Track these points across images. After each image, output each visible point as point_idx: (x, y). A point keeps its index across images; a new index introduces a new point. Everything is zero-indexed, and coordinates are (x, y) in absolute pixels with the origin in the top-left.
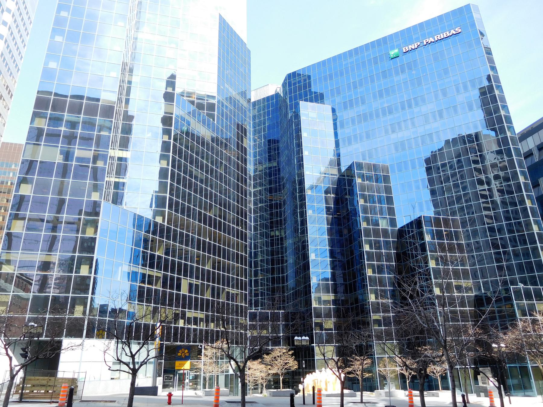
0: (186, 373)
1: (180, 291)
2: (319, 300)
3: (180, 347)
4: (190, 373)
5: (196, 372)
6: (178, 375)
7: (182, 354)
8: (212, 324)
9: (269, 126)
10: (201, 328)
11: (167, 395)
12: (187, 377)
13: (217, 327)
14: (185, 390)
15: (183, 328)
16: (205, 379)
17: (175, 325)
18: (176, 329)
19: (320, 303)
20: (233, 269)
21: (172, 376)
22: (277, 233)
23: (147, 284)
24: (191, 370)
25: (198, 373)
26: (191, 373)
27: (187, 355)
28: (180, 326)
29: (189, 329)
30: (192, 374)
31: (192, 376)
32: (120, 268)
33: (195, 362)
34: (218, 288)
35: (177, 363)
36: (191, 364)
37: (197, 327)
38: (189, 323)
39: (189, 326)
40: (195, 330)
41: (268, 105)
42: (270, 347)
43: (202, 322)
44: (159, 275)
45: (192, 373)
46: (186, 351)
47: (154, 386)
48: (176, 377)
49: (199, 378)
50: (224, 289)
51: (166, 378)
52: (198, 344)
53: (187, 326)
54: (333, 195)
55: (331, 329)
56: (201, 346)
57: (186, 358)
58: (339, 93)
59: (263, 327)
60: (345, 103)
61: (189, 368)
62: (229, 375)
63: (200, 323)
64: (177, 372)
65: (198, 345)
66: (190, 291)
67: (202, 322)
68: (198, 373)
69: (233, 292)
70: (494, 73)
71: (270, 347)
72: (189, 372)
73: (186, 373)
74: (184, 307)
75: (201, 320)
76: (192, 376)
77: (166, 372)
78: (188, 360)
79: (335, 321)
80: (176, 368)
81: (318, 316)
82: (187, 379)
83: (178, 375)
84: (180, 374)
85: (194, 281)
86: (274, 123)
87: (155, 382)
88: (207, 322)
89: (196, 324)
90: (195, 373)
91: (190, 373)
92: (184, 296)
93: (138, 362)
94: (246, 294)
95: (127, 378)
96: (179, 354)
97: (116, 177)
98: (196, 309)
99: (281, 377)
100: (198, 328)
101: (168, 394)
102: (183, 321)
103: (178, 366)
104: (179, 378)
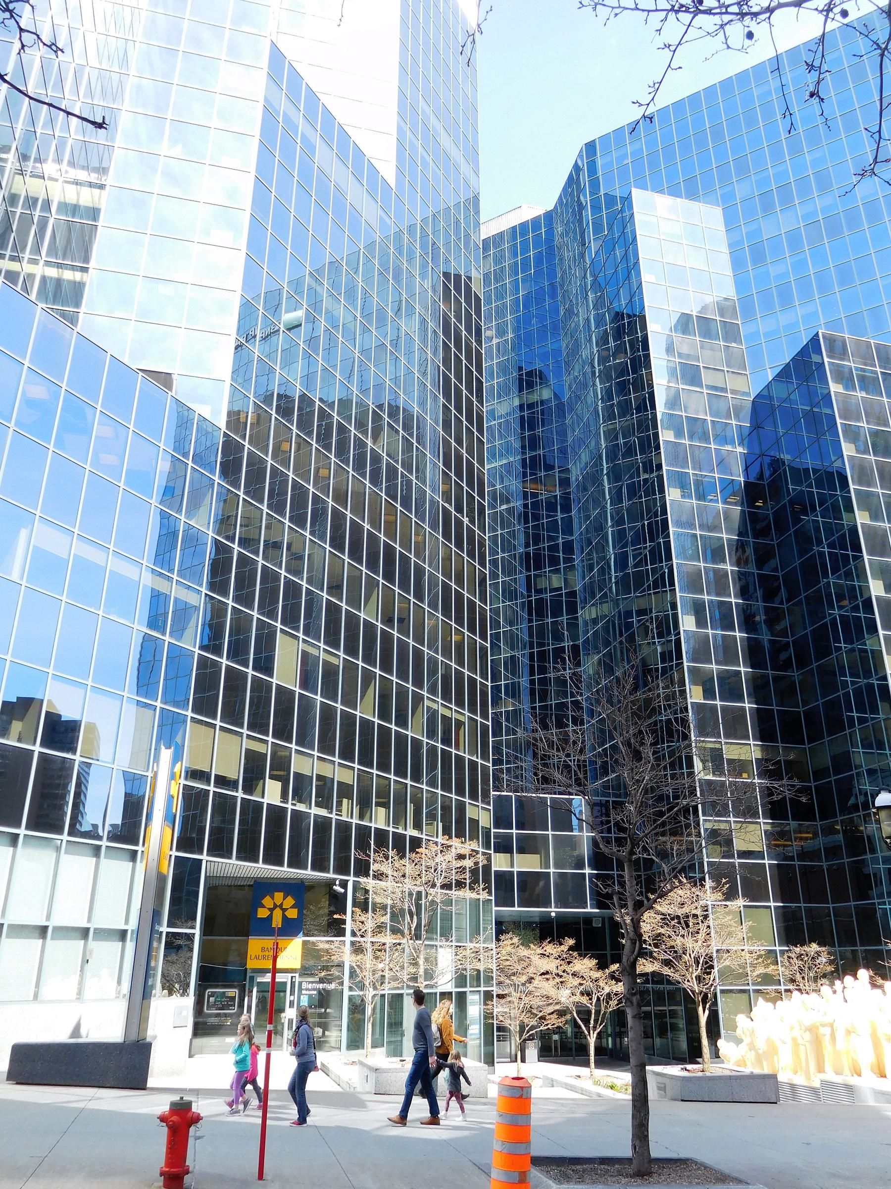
0: (285, 984)
1: (269, 671)
2: (715, 759)
3: (264, 887)
4: (300, 984)
5: (322, 981)
6: (255, 990)
7: (271, 910)
8: (382, 811)
9: (527, 298)
10: (344, 818)
11: (163, 1119)
12: (289, 998)
13: (396, 822)
14: (280, 1046)
15: (276, 814)
16: (357, 1008)
17: (251, 794)
18: (252, 810)
19: (718, 768)
20: (433, 672)
21: (233, 992)
22: (557, 581)
23: (138, 623)
24: (305, 971)
25: (332, 986)
26: (304, 986)
27: (293, 914)
28: (266, 801)
29: (298, 816)
30: (310, 988)
31: (310, 996)
32: (24, 534)
33: (321, 941)
34: (402, 693)
35: (256, 945)
36: (309, 951)
37: (331, 813)
38: (300, 795)
39: (301, 807)
40: (323, 825)
41: (525, 244)
42: (553, 909)
43: (345, 801)
44: (192, 599)
45: (310, 986)
46: (290, 901)
47: (133, 1037)
48: (250, 997)
49: (332, 1004)
50: (418, 699)
51: (212, 999)
52: (331, 875)
53: (293, 804)
54: (740, 450)
55: (760, 855)
56: (344, 884)
57: (290, 928)
58: (743, 170)
59: (527, 846)
60: (765, 196)
61: (297, 965)
62: (436, 994)
63: (339, 804)
64: (252, 979)
65: (332, 882)
66: (307, 681)
67: (345, 801)
68: (332, 986)
69: (448, 713)
70: (858, 451)
71: (553, 909)
72: (297, 980)
73: (285, 984)
74: (282, 732)
75: (345, 791)
76: (310, 996)
77: (207, 977)
78: (295, 934)
79: (769, 827)
80: (251, 964)
81: (717, 809)
82: (291, 1004)
83: (255, 990)
84: (262, 987)
85: (321, 650)
86: (542, 288)
87: (136, 1020)
88: (365, 806)
89: (324, 801)
90: (321, 986)
91: (300, 984)
92: (285, 695)
93: (88, 929)
94: (485, 728)
95: (74, 996)
96: (262, 913)
97: (47, 263)
98: (326, 747)
99: (700, 1009)
100: (333, 816)
101: (165, 1108)
102: (278, 785)
103: (257, 958)
104: (261, 1001)
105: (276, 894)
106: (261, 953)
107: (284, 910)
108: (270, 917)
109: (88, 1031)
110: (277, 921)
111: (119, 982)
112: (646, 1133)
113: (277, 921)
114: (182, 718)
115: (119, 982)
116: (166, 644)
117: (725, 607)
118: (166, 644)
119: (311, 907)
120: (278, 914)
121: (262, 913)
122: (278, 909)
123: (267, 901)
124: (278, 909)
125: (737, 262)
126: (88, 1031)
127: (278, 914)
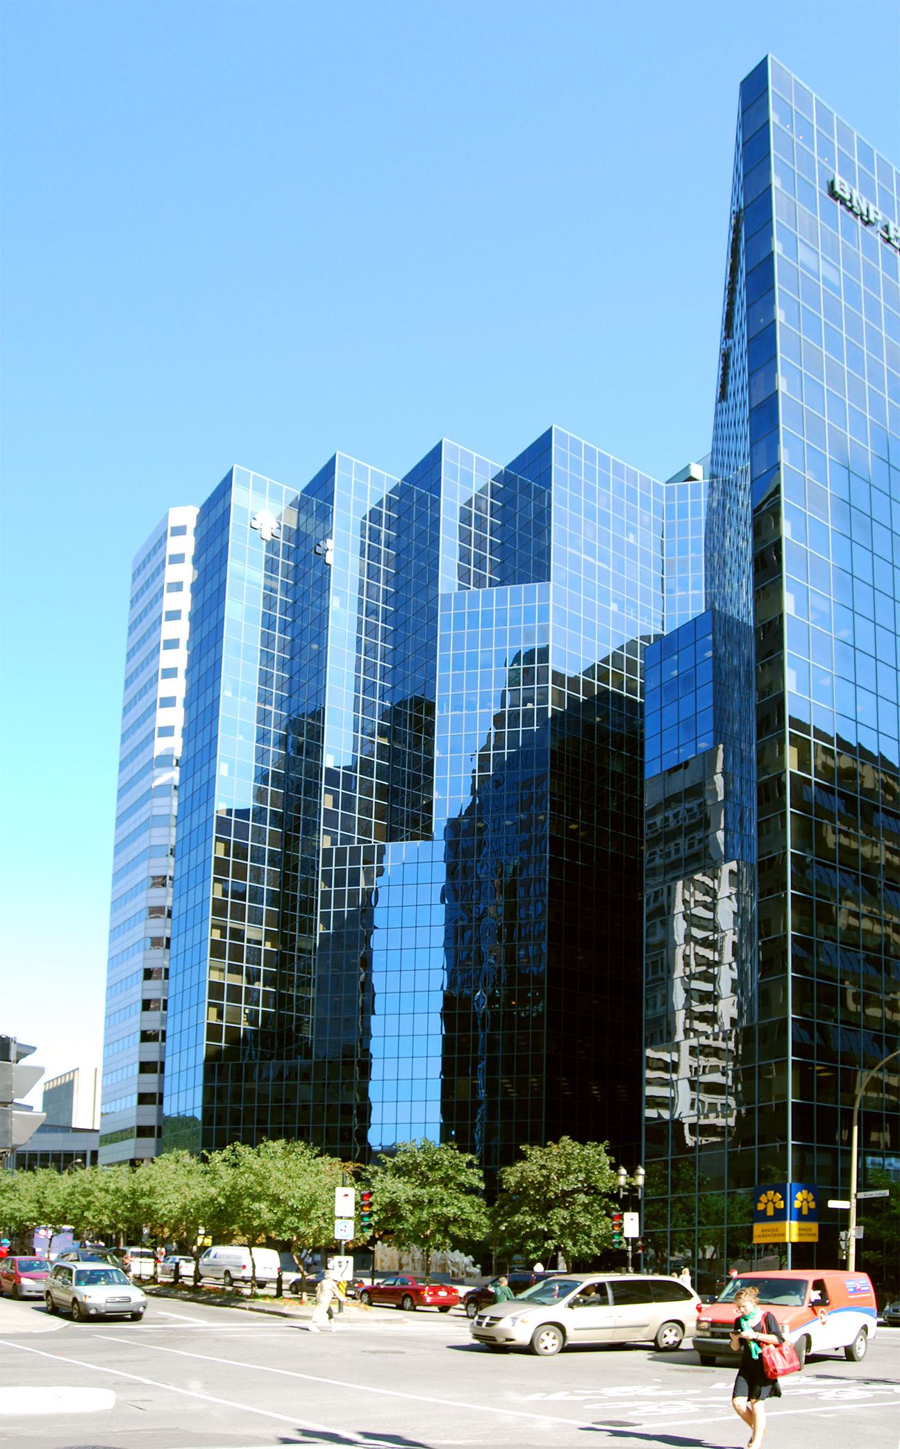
7: (766, 1204)
96: (761, 1207)
103: (759, 1236)
105: (769, 1192)
106: (762, 1234)
107: (774, 1203)
108: (766, 1208)
109: (448, 1347)
110: (770, 1212)
111: (37, 1292)
112: (88, 1273)
113: (770, 1212)
114: (260, 890)
115: (37, 1292)
116: (269, 792)
117: (457, 707)
118: (269, 792)
119: (642, 1171)
120: (770, 1206)
121: (761, 1207)
122: (770, 1203)
123: (763, 1198)
124: (770, 1203)
125: (714, 676)
126: (448, 1347)
127: (770, 1206)
